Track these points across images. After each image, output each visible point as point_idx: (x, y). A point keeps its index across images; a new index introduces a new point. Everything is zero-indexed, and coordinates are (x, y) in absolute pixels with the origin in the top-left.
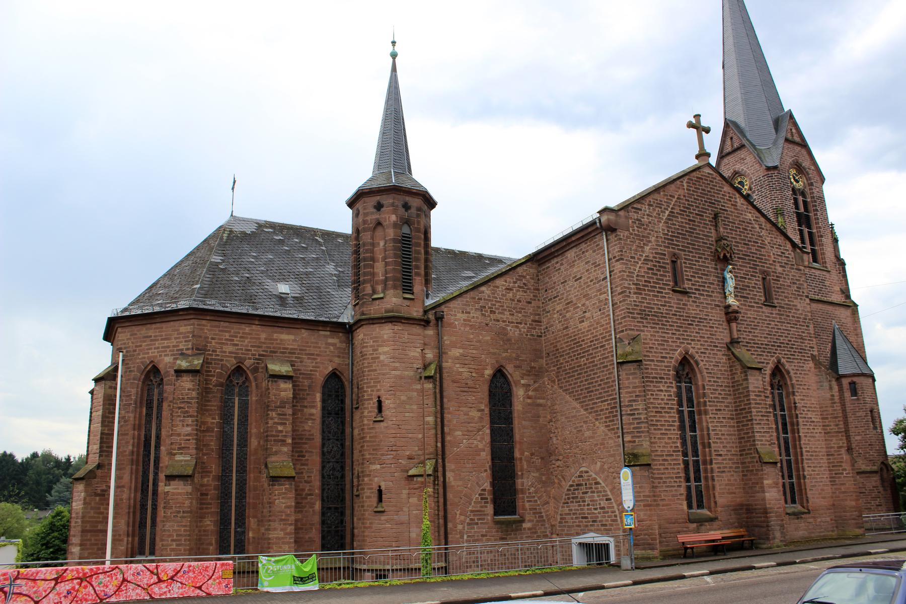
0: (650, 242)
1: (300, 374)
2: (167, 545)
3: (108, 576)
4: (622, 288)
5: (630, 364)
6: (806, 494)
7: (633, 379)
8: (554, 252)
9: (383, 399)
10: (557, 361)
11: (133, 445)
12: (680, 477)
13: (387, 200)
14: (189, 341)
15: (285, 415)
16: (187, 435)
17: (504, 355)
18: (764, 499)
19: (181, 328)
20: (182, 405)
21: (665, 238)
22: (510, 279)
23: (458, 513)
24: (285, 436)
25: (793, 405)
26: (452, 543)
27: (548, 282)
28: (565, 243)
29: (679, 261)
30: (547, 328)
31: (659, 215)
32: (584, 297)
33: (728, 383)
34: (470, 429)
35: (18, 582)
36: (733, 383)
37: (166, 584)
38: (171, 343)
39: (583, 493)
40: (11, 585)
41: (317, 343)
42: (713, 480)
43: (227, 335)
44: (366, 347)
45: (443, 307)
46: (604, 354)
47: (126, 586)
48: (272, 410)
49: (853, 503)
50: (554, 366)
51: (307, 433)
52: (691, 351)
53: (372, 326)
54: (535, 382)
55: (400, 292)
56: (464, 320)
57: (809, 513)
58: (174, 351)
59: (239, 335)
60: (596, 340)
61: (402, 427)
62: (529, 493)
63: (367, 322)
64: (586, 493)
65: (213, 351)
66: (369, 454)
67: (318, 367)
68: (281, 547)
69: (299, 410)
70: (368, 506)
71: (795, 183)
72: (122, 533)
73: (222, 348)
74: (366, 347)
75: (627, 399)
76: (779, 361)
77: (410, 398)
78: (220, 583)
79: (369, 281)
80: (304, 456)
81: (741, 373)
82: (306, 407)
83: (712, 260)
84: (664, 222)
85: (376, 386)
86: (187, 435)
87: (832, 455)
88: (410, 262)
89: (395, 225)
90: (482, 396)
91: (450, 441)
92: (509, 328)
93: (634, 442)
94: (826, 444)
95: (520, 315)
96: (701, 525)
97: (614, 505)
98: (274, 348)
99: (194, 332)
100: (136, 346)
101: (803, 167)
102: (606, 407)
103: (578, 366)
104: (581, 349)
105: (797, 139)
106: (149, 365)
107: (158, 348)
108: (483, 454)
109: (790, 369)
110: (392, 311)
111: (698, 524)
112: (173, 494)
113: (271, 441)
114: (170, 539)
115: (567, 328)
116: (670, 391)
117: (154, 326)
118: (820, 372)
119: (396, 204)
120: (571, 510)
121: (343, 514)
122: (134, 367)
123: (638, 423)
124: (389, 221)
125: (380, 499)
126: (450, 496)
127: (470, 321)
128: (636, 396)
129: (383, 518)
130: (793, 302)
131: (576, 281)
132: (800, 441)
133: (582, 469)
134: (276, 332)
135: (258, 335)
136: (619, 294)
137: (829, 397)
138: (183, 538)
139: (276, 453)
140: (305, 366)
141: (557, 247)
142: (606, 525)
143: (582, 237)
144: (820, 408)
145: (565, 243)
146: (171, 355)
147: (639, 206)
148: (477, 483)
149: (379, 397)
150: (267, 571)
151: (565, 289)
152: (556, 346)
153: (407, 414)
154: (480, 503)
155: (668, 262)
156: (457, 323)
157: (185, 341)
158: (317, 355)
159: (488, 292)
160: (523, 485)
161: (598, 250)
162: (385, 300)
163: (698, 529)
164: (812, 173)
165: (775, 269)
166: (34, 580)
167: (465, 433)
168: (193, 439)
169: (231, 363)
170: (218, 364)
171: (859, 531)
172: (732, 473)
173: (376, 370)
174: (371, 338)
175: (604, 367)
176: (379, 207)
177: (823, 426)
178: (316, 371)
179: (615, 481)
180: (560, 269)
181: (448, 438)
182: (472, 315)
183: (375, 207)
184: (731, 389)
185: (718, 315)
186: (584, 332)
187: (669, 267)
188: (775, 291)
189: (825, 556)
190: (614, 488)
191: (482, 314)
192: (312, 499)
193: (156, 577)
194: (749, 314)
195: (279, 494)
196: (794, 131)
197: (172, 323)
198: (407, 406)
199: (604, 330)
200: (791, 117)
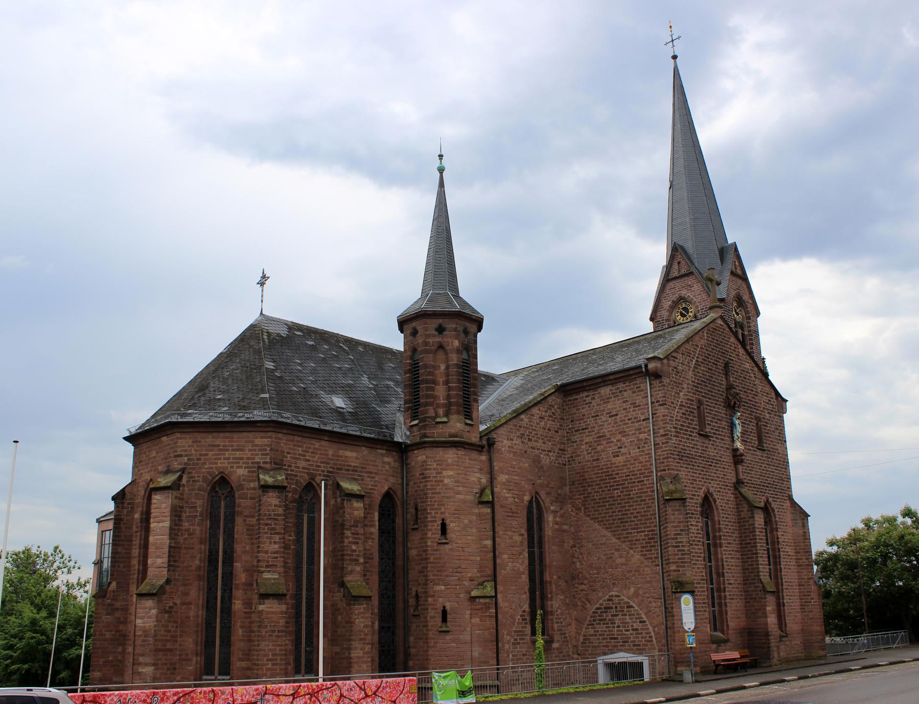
0: (683, 388)
2: (264, 665)
3: (330, 692)
4: (665, 431)
5: (675, 501)
6: (785, 619)
7: (678, 514)
8: (586, 386)
9: (447, 522)
10: (584, 490)
11: (200, 560)
13: (450, 325)
14: (267, 454)
15: (358, 534)
16: (275, 553)
17: (539, 481)
18: (766, 624)
19: (256, 440)
20: (269, 522)
21: (693, 385)
22: (542, 408)
23: (505, 633)
24: (358, 556)
25: (776, 540)
27: (575, 414)
28: (600, 380)
29: (702, 407)
30: (572, 457)
31: (689, 363)
32: (620, 433)
33: (735, 519)
35: (267, 696)
36: (739, 519)
37: (371, 699)
38: (244, 454)
39: (612, 616)
40: (262, 699)
41: (375, 461)
42: (726, 606)
44: (430, 469)
45: (493, 433)
46: (642, 489)
47: (343, 701)
48: (347, 529)
50: (580, 495)
52: (711, 490)
54: (561, 509)
55: (462, 417)
56: (509, 447)
57: (787, 636)
58: (248, 463)
59: (310, 451)
60: (633, 475)
62: (557, 615)
63: (431, 445)
64: (617, 615)
65: (289, 466)
66: (433, 575)
67: (376, 486)
68: (360, 667)
70: (432, 626)
71: (736, 316)
73: (296, 463)
74: (430, 469)
75: (673, 533)
77: (471, 522)
78: (408, 697)
79: (432, 404)
81: (748, 511)
83: (724, 407)
85: (440, 509)
86: (275, 553)
88: (468, 388)
89: (458, 351)
92: (542, 456)
93: (679, 571)
94: (798, 576)
95: (550, 443)
96: (719, 646)
97: (649, 626)
98: (340, 465)
99: (271, 445)
100: (201, 455)
101: (744, 301)
102: (643, 537)
103: (610, 497)
104: (614, 482)
105: (739, 272)
106: (217, 476)
107: (229, 459)
108: (523, 576)
110: (457, 436)
112: (268, 613)
113: (347, 560)
114: (265, 659)
115: (598, 459)
117: (222, 435)
118: (795, 510)
119: (458, 329)
120: (598, 631)
121: (394, 633)
122: (198, 477)
123: (682, 554)
124: (452, 346)
125: (444, 619)
127: (513, 448)
128: (681, 530)
130: (776, 446)
131: (610, 417)
132: (781, 572)
133: (614, 593)
136: (662, 436)
137: (802, 533)
138: (279, 658)
139: (351, 572)
141: (593, 382)
142: (639, 645)
144: (795, 543)
145: (600, 380)
146: (245, 468)
147: (675, 354)
148: (519, 605)
149: (443, 520)
150: (438, 686)
151: (596, 423)
152: (584, 476)
153: (469, 538)
154: (522, 623)
155: (695, 407)
156: (503, 449)
157: (262, 454)
158: (376, 474)
159: (526, 420)
160: (552, 607)
161: (639, 391)
162: (448, 424)
163: (717, 649)
164: (750, 308)
165: (764, 415)
166: (278, 695)
168: (281, 557)
169: (304, 479)
170: (293, 480)
171: (821, 653)
172: (738, 600)
174: (435, 461)
175: (641, 501)
176: (440, 330)
177: (797, 559)
178: (374, 490)
179: (650, 605)
180: (590, 403)
182: (514, 442)
183: (436, 330)
184: (737, 525)
185: (728, 458)
186: (619, 466)
188: (765, 436)
189: (826, 672)
190: (650, 611)
193: (363, 692)
194: (748, 457)
195: (359, 614)
196: (737, 263)
197: (245, 433)
198: (469, 530)
199: (642, 466)
200: (736, 250)
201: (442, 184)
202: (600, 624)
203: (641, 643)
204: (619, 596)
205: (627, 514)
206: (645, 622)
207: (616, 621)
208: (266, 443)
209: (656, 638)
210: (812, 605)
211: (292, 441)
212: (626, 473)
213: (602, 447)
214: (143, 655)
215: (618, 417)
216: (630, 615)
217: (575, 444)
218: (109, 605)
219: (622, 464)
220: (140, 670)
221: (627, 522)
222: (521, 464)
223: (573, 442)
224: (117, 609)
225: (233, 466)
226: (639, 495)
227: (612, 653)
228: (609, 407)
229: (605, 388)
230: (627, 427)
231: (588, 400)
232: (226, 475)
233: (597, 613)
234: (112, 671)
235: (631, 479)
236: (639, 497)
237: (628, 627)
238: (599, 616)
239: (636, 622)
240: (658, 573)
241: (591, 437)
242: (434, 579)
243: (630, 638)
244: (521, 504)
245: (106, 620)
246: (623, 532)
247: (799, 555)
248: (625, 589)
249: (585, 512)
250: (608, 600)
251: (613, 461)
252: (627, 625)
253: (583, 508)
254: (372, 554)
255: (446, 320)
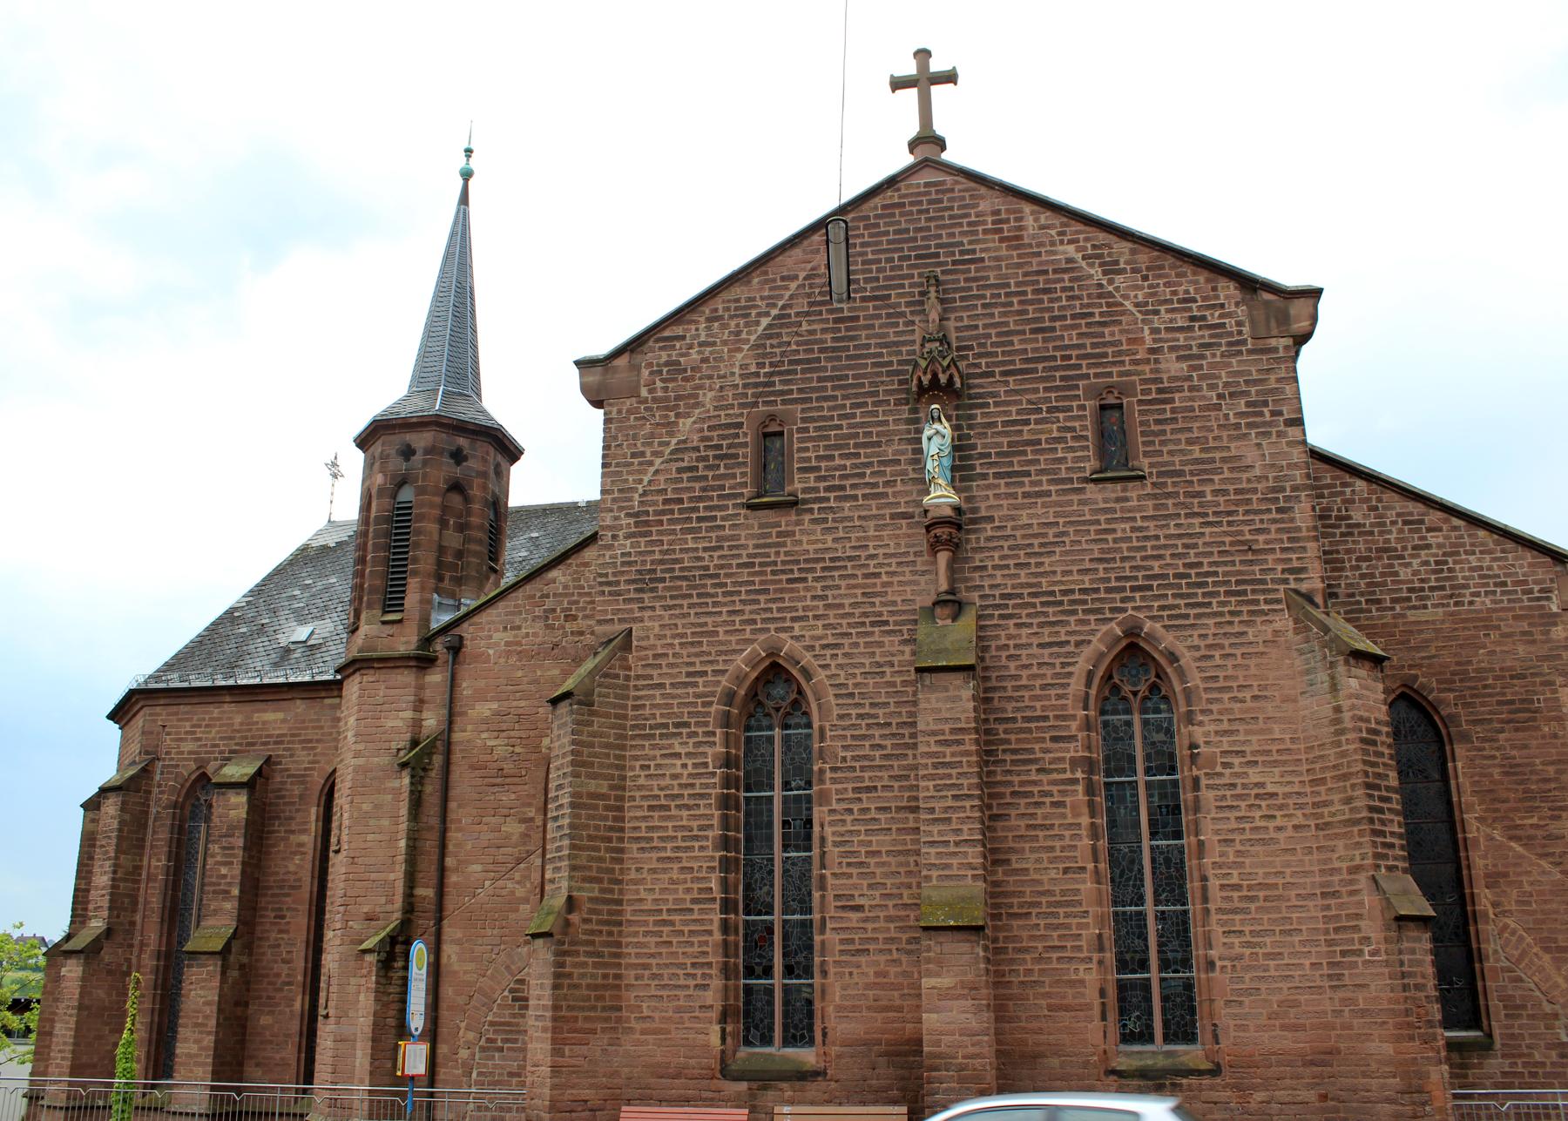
1: (289, 776)
12: (709, 965)
13: (421, 440)
15: (233, 848)
23: (463, 1025)
24: (230, 884)
26: (446, 1083)
34: (500, 858)
41: (319, 720)
43: (187, 726)
49: (1388, 1049)
51: (292, 877)
52: (789, 646)
56: (508, 644)
57: (1216, 1071)
61: (359, 861)
67: (318, 762)
68: (191, 1071)
69: (283, 839)
73: (179, 747)
76: (1132, 631)
80: (283, 917)
82: (293, 832)
84: (752, 348)
87: (1335, 894)
90: (532, 792)
91: (456, 884)
109: (1180, 648)
111: (755, 1085)
116: (704, 754)
126: (447, 991)
127: (519, 643)
134: (258, 711)
135: (230, 718)
137: (1331, 714)
139: (215, 912)
140: (296, 762)
153: (370, 837)
156: (491, 652)
158: (318, 741)
167: (491, 867)
169: (188, 769)
170: (172, 773)
172: (895, 955)
181: (453, 878)
182: (524, 631)
187: (747, 453)
191: (547, 627)
192: (290, 991)
195: (198, 981)
198: (372, 822)
201: (464, 199)
210: (1366, 962)
211: (176, 714)
222: (539, 673)
244: (534, 756)
247: (1322, 789)
254: (299, 880)
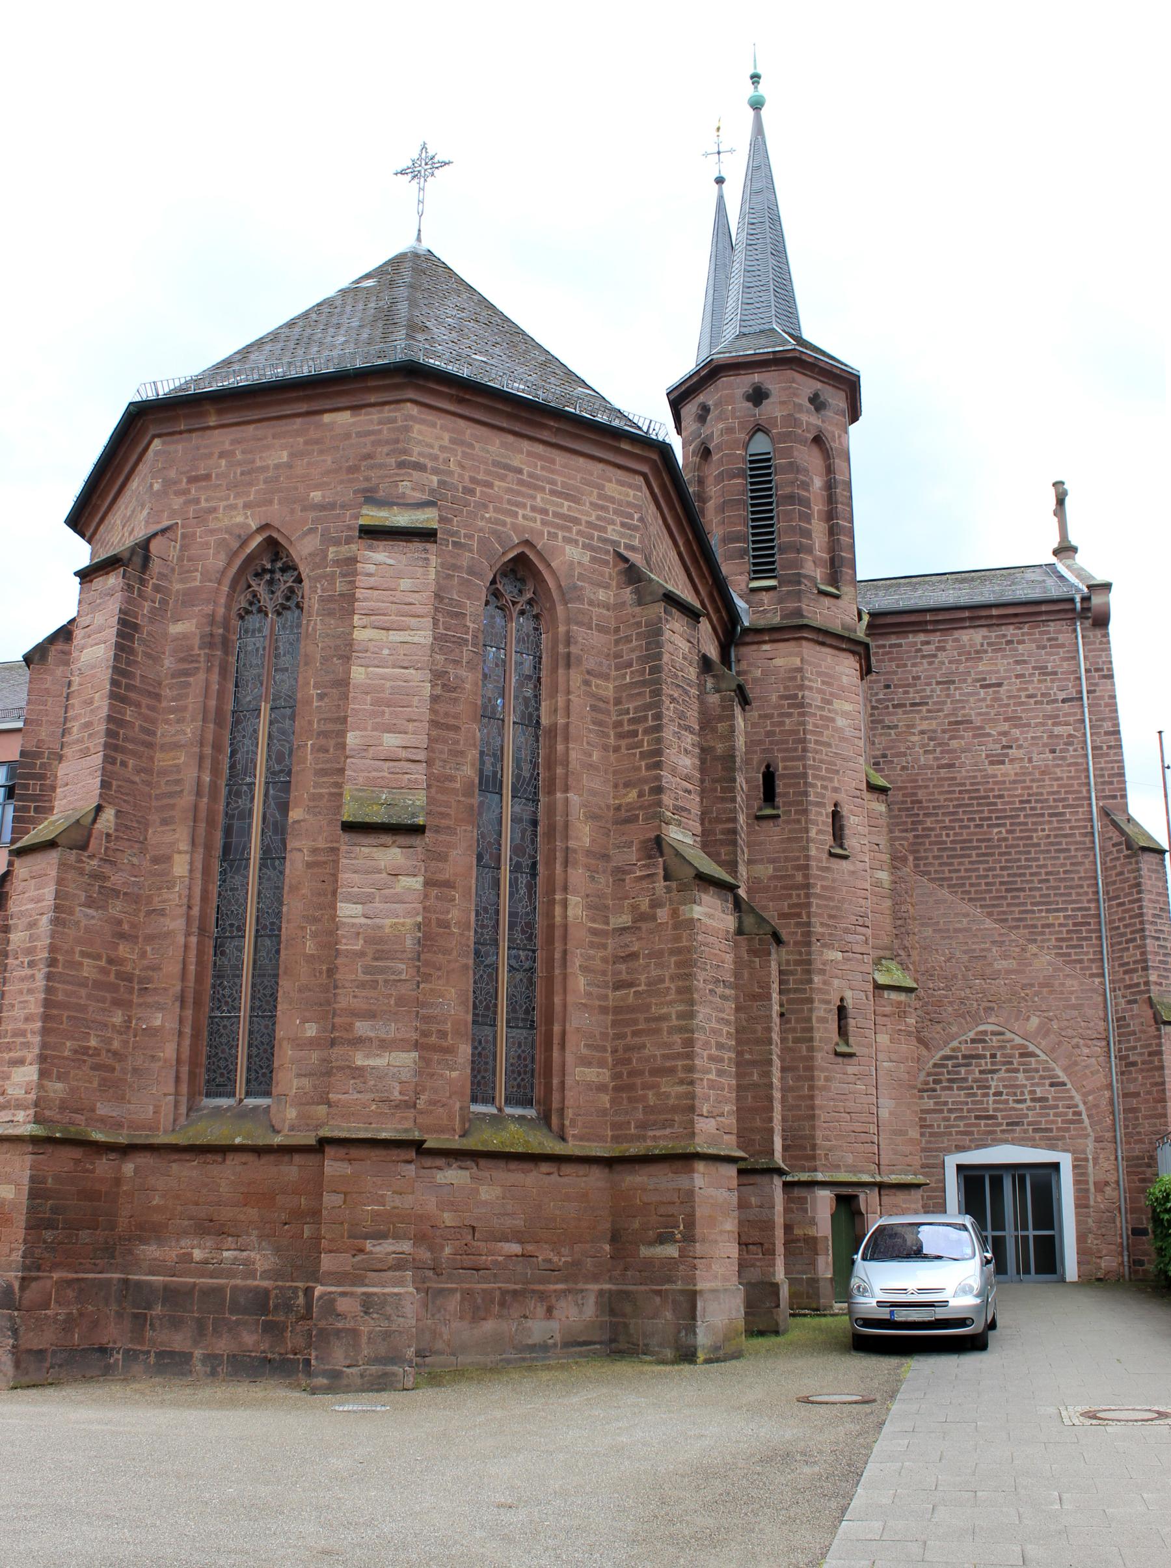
8: (926, 622)
9: (845, 811)
19: (607, 484)
30: (884, 756)
32: (1006, 720)
53: (818, 648)
72: (448, 1027)
75: (1151, 912)
97: (1074, 1093)
102: (1062, 921)
125: (843, 1032)
129: (850, 1069)
131: (982, 687)
141: (947, 616)
143: (1016, 615)
145: (967, 614)
149: (836, 805)
151: (948, 696)
152: (915, 794)
173: (829, 745)
174: (819, 674)
183: (749, 398)
190: (1076, 1063)
197: (581, 460)
202: (950, 1088)
203: (1054, 1127)
204: (1002, 1034)
205: (1024, 875)
206: (1064, 1084)
207: (993, 1084)
208: (631, 499)
209: (1089, 1116)
212: (1021, 795)
213: (963, 742)
214: (371, 1015)
215: (1002, 689)
216: (1025, 1071)
217: (892, 732)
218: (96, 876)
219: (1013, 778)
220: (360, 1061)
221: (1023, 890)
223: (889, 727)
224: (116, 893)
225: (555, 536)
226: (1052, 840)
227: (978, 1147)
228: (981, 668)
229: (972, 631)
230: (1024, 711)
231: (928, 649)
232: (539, 554)
233: (943, 1066)
234: (95, 1084)
235: (1032, 809)
236: (1051, 844)
237: (1022, 1093)
238: (949, 1073)
239: (1043, 1085)
240: (1094, 991)
241: (934, 722)
242: (823, 935)
243: (1026, 1116)
245: (84, 922)
246: (1013, 909)
248: (1017, 1019)
249: (916, 866)
250: (973, 1041)
251: (990, 772)
252: (1018, 1091)
253: (911, 858)
255: (830, 389)
